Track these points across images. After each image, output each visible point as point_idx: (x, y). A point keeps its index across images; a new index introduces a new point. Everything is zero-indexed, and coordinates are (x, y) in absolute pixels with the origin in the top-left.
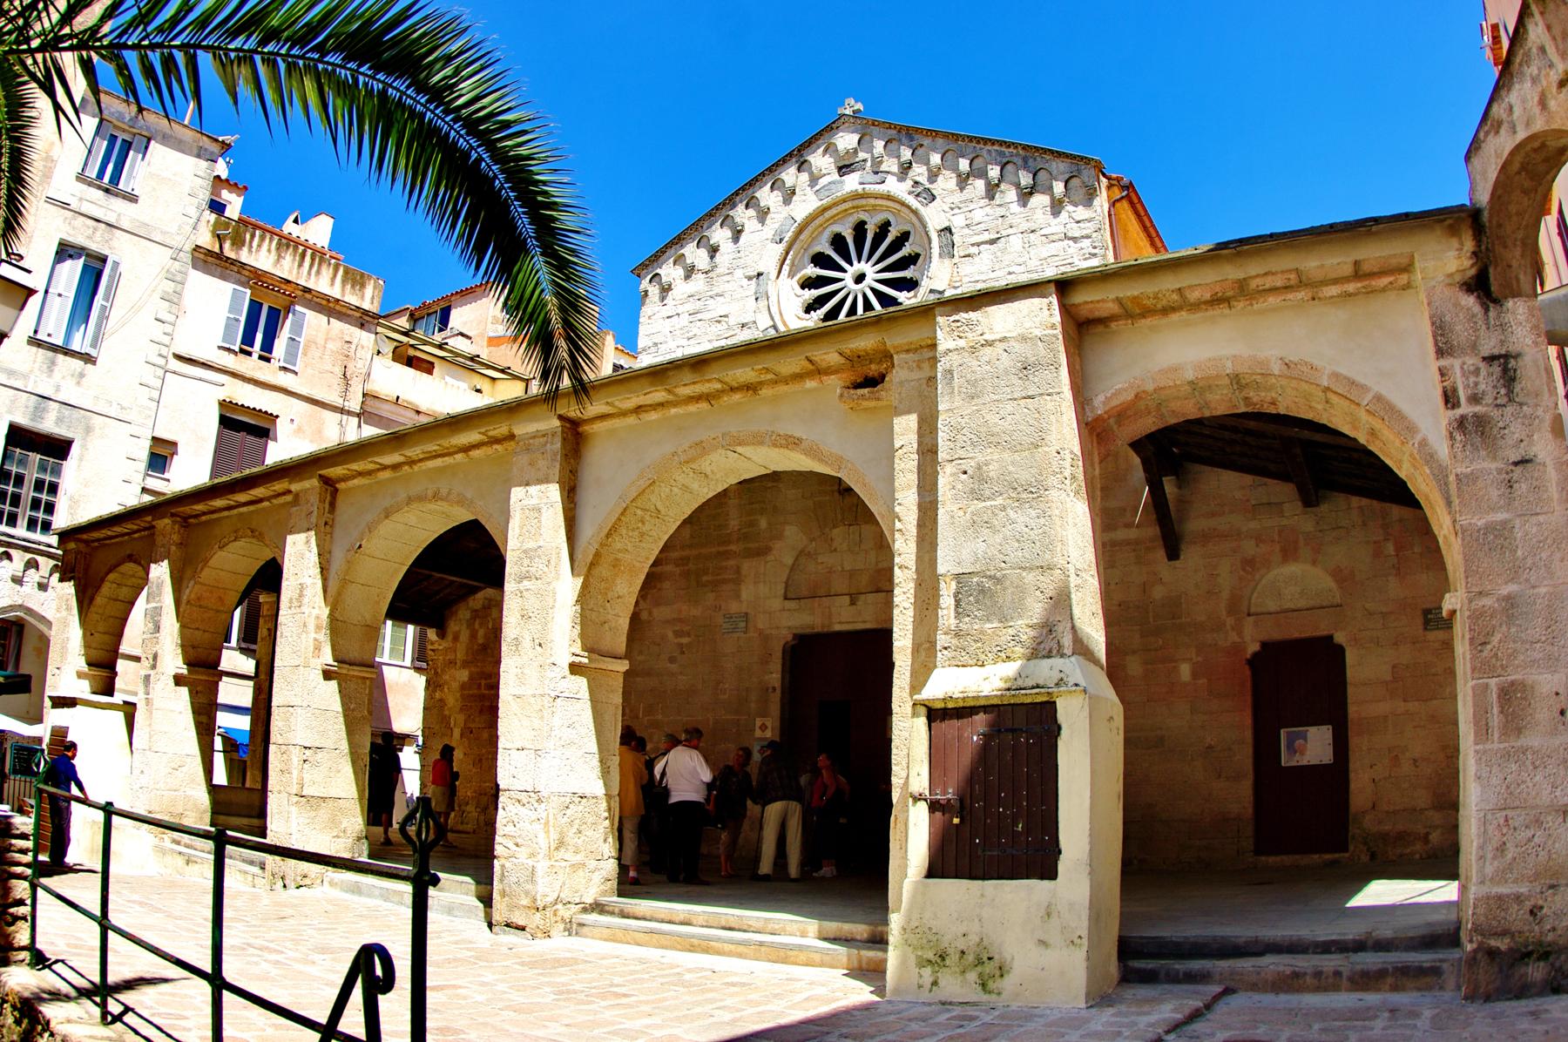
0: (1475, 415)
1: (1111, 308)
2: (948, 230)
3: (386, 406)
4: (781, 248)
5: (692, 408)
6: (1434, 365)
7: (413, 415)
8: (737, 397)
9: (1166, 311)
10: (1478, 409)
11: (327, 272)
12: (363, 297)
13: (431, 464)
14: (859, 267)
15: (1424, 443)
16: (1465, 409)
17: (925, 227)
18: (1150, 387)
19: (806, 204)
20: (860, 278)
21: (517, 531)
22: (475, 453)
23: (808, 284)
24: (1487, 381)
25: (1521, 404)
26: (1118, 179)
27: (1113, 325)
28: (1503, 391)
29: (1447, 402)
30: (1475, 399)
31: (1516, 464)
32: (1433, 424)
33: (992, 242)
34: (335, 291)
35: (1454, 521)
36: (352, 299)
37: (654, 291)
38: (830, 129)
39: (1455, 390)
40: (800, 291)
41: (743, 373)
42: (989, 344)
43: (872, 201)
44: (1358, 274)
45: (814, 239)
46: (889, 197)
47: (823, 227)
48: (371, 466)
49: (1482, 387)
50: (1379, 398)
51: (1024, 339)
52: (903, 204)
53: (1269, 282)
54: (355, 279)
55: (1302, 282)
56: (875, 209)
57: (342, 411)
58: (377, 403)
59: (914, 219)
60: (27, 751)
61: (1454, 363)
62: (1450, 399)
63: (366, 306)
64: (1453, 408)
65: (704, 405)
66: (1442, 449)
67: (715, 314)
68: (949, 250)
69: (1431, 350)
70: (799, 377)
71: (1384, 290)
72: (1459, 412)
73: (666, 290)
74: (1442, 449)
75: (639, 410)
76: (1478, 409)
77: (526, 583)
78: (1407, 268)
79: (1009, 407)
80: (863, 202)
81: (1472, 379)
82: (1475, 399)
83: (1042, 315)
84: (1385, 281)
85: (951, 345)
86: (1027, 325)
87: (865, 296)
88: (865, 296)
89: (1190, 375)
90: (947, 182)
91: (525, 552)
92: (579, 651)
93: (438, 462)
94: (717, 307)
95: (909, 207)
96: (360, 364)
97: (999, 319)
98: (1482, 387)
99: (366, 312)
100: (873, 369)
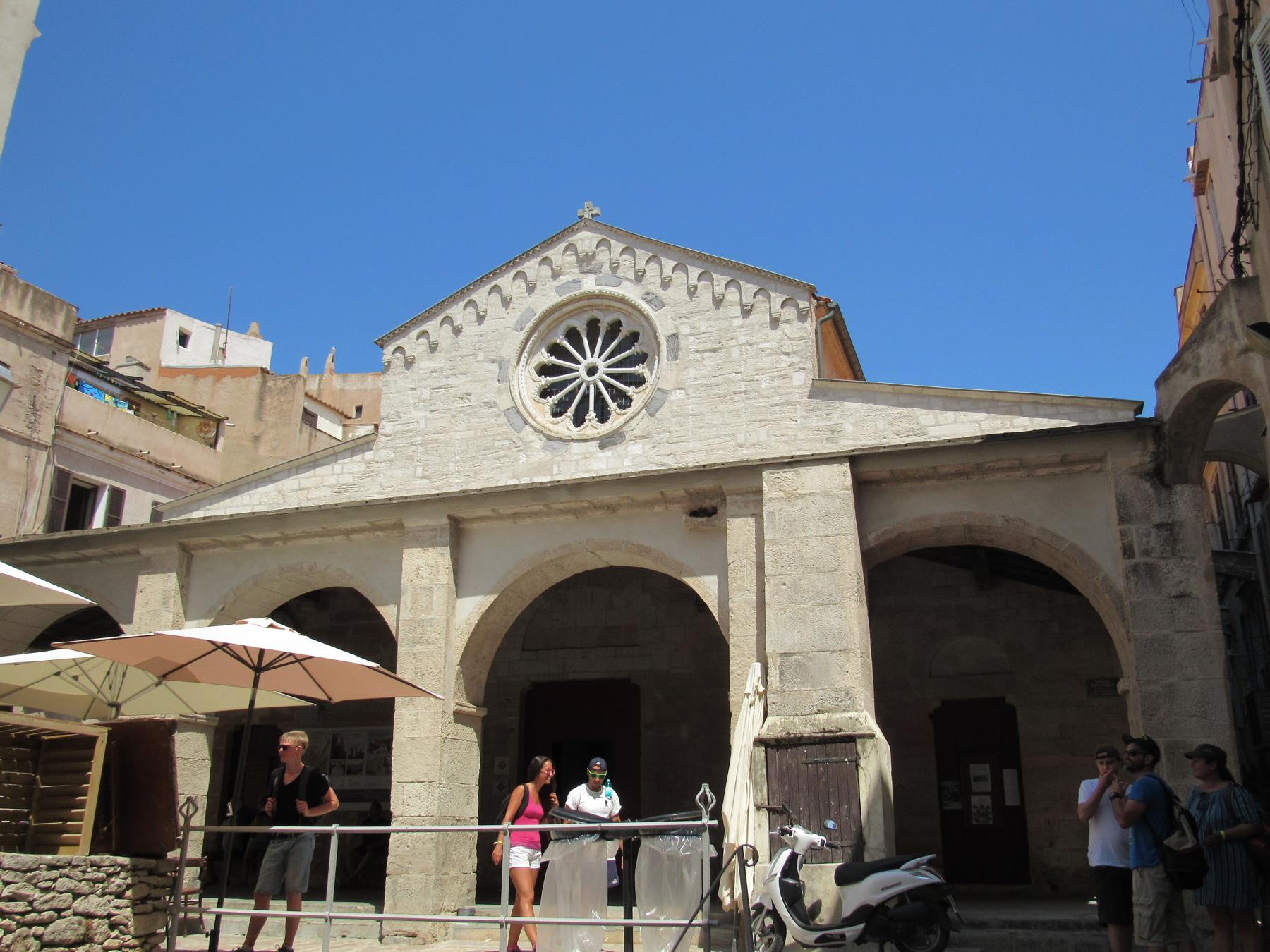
0: (1146, 563)
1: (885, 475)
2: (676, 336)
3: (80, 441)
4: (522, 336)
5: (561, 518)
6: (1115, 528)
7: (105, 450)
8: (599, 513)
9: (922, 478)
10: (1147, 559)
11: (14, 294)
12: (54, 324)
13: (306, 542)
14: (591, 360)
15: (1105, 579)
16: (1139, 558)
17: (655, 332)
18: (908, 530)
19: (547, 297)
20: (592, 371)
21: (409, 604)
22: (355, 537)
23: (544, 370)
24: (1154, 541)
25: (1182, 558)
26: (827, 301)
27: (884, 486)
28: (1168, 548)
29: (1124, 554)
30: (1146, 553)
31: (1176, 597)
32: (1112, 566)
33: (714, 351)
34: (25, 315)
35: (1128, 632)
36: (45, 326)
37: (398, 360)
38: (570, 230)
39: (1131, 546)
40: (537, 377)
41: (609, 497)
42: (801, 496)
43: (606, 302)
44: (1064, 462)
45: (550, 330)
46: (622, 300)
47: (559, 321)
48: (239, 538)
49: (1152, 544)
50: (1073, 547)
51: (826, 494)
52: (635, 307)
53: (999, 464)
54: (47, 304)
55: (1022, 465)
56: (608, 308)
57: (26, 442)
58: (69, 436)
59: (644, 323)
60: (54, 756)
61: (1133, 529)
62: (1127, 551)
63: (58, 332)
64: (1129, 558)
65: (571, 518)
66: (1120, 584)
67: (459, 392)
68: (674, 353)
69: (1115, 517)
70: (650, 503)
71: (1081, 472)
72: (1133, 561)
73: (409, 364)
74: (1120, 584)
75: (515, 516)
76: (1147, 559)
77: (419, 647)
78: (1101, 460)
79: (815, 542)
80: (598, 302)
81: (1145, 539)
82: (1146, 553)
83: (841, 476)
84: (1083, 467)
85: (774, 494)
86: (829, 486)
87: (597, 388)
88: (597, 388)
89: (937, 524)
90: (676, 293)
91: (417, 622)
92: (464, 702)
93: (316, 541)
94: (461, 384)
95: (640, 311)
96: (50, 394)
97: (812, 477)
98: (1152, 544)
99: (58, 340)
100: (707, 503)
